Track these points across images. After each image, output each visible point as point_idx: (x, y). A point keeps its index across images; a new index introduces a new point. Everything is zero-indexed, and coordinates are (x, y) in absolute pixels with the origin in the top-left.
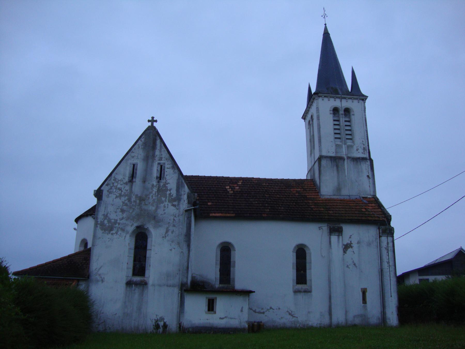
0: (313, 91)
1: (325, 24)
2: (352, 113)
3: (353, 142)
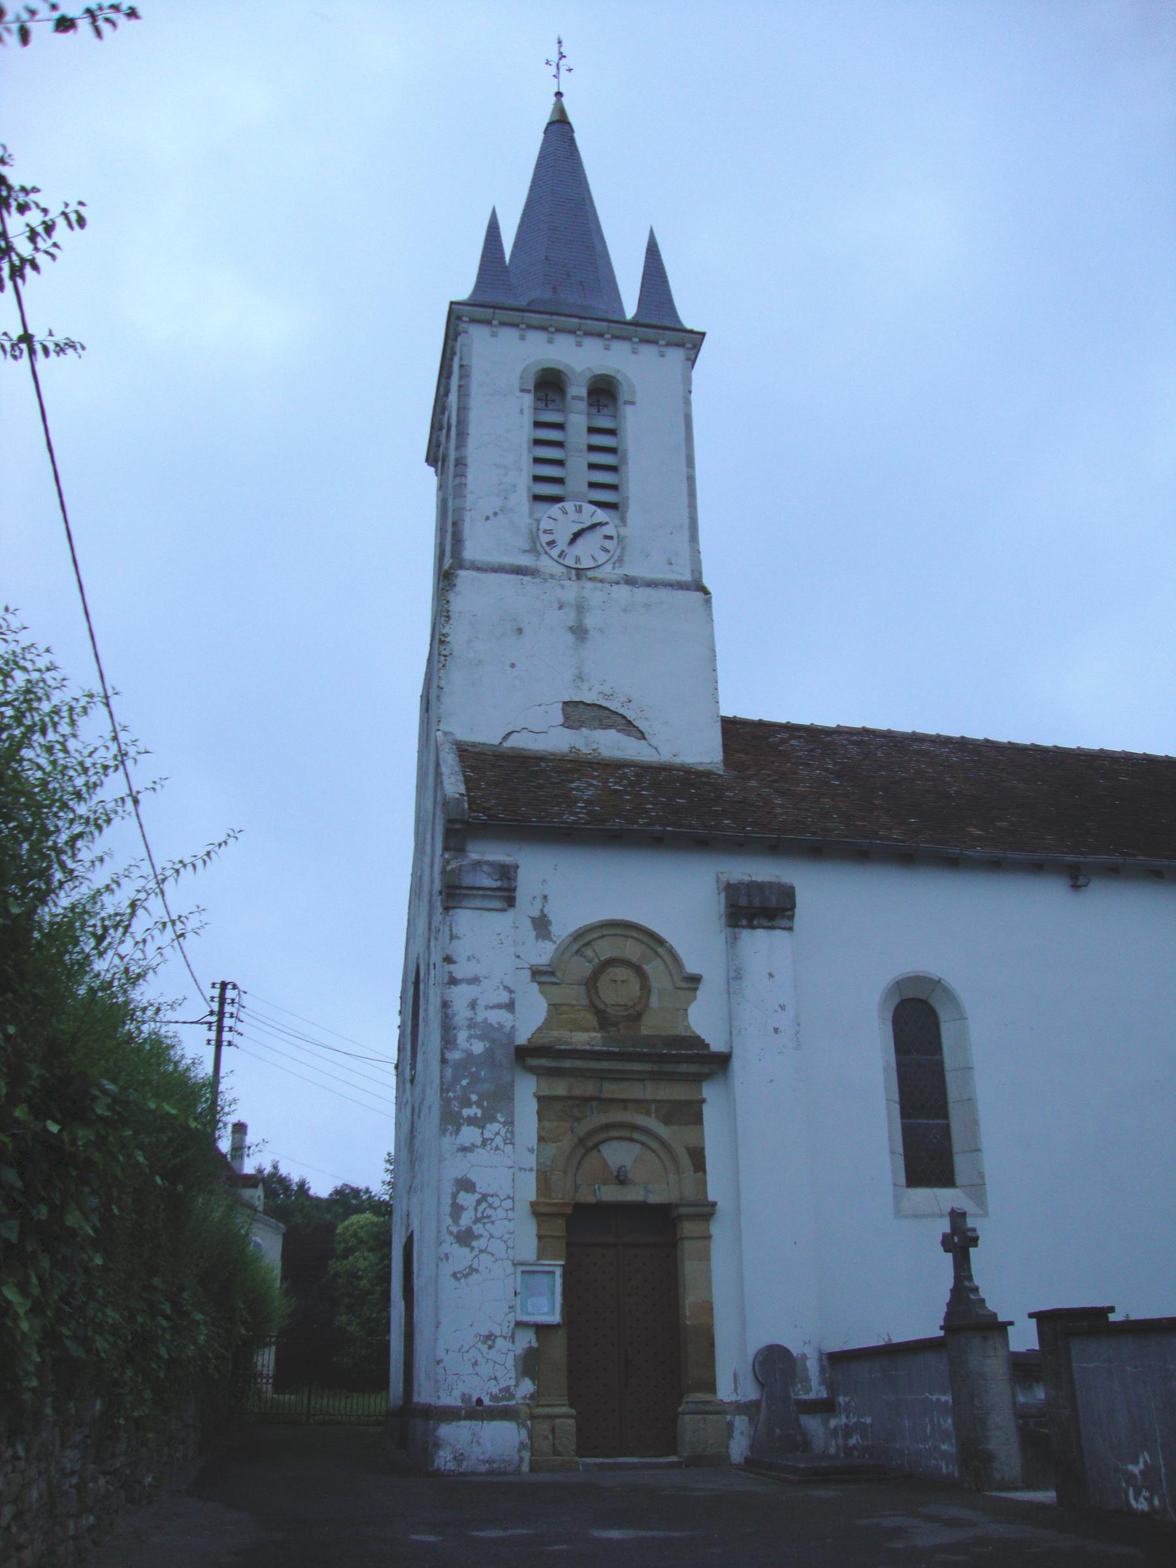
0: (1112, 1317)
1: (559, 94)
2: (624, 396)
3: (623, 520)
